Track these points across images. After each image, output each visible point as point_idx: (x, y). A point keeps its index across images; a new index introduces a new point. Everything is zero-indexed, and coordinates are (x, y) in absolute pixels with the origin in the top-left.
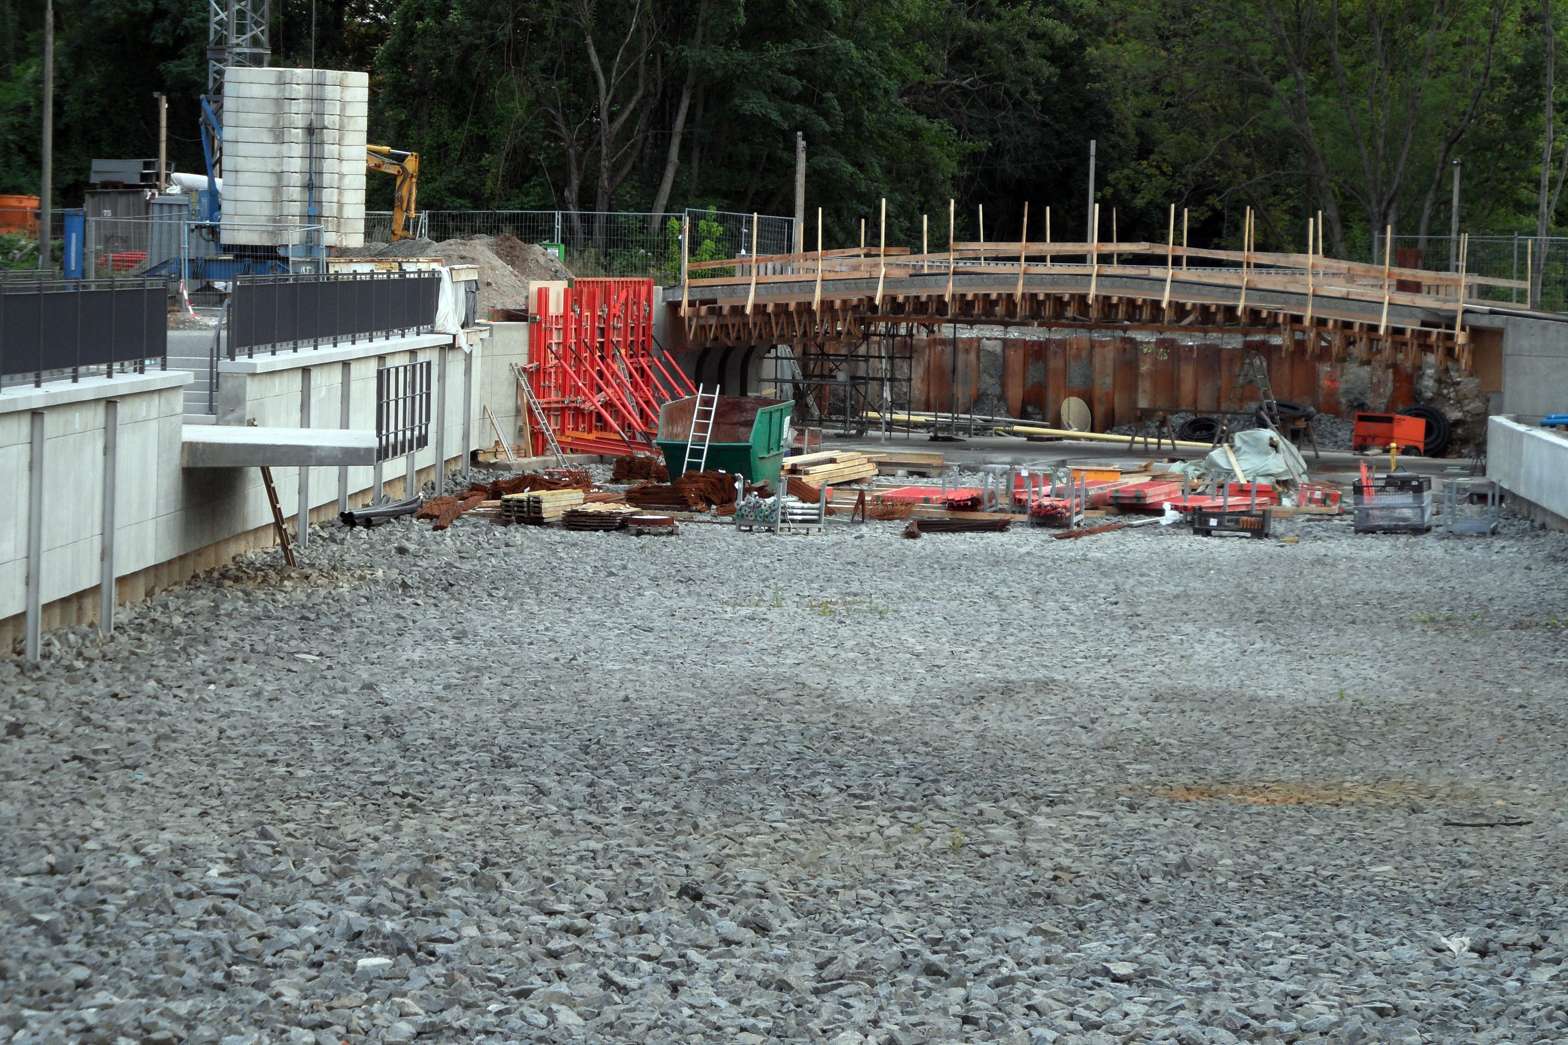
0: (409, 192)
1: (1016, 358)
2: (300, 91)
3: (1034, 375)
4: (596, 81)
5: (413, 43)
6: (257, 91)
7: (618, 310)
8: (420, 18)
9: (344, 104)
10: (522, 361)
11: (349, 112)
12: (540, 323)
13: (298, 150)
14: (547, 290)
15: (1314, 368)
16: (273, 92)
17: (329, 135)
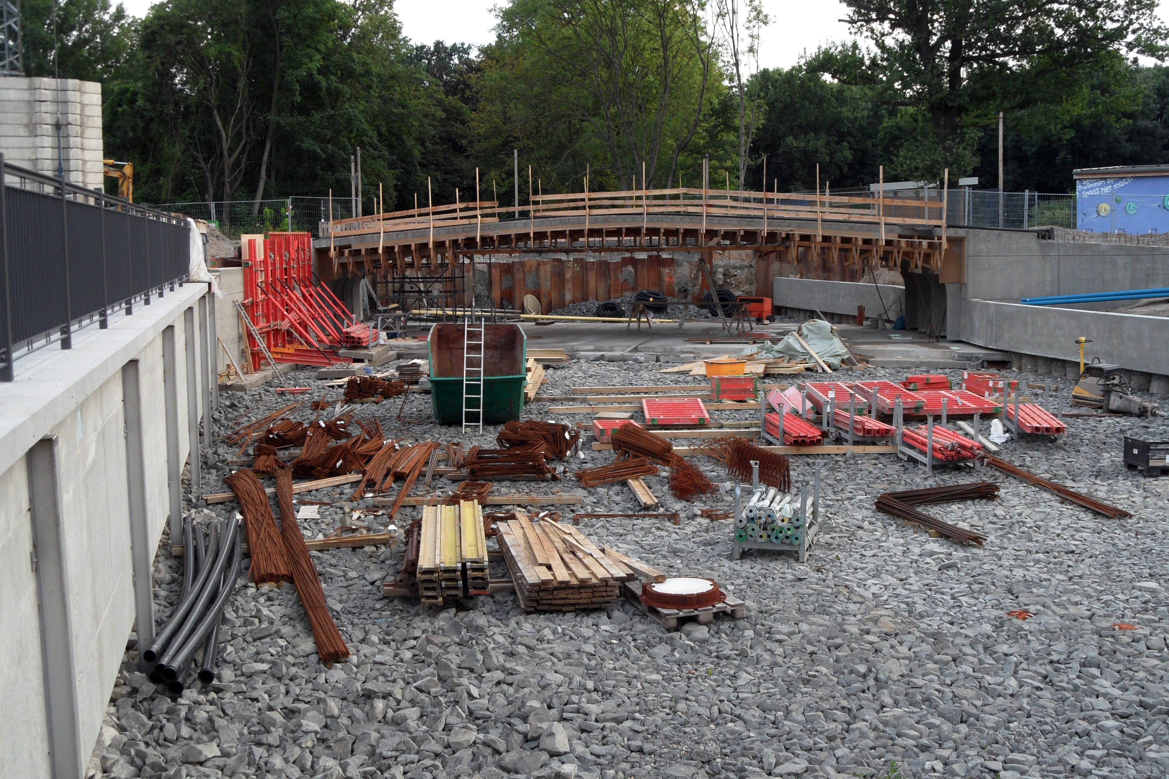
0: (127, 188)
1: (496, 273)
2: (48, 95)
3: (506, 284)
4: (219, 137)
5: (117, 120)
6: (12, 95)
7: (294, 255)
8: (120, 105)
9: (83, 106)
10: (239, 297)
11: (87, 112)
12: (251, 267)
13: (48, 141)
14: (254, 240)
15: (659, 271)
16: (26, 96)
17: (73, 130)
